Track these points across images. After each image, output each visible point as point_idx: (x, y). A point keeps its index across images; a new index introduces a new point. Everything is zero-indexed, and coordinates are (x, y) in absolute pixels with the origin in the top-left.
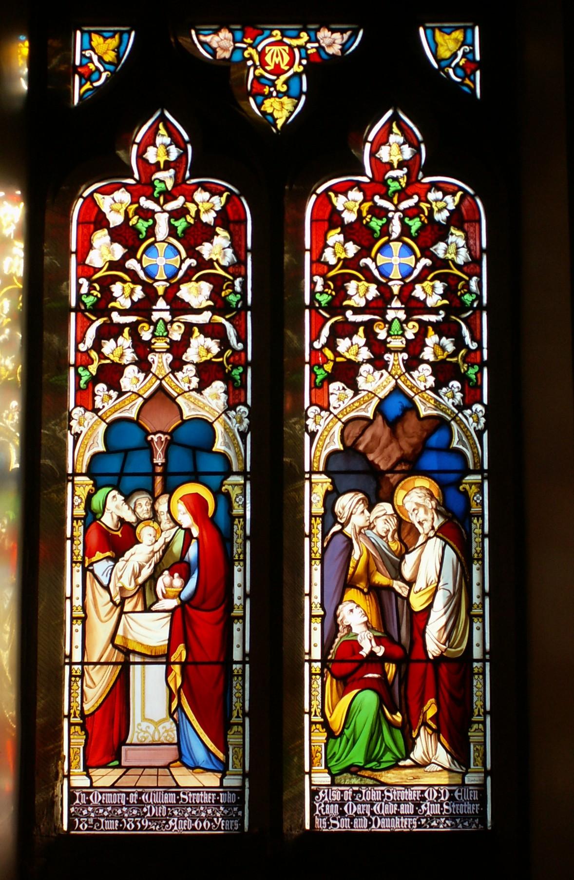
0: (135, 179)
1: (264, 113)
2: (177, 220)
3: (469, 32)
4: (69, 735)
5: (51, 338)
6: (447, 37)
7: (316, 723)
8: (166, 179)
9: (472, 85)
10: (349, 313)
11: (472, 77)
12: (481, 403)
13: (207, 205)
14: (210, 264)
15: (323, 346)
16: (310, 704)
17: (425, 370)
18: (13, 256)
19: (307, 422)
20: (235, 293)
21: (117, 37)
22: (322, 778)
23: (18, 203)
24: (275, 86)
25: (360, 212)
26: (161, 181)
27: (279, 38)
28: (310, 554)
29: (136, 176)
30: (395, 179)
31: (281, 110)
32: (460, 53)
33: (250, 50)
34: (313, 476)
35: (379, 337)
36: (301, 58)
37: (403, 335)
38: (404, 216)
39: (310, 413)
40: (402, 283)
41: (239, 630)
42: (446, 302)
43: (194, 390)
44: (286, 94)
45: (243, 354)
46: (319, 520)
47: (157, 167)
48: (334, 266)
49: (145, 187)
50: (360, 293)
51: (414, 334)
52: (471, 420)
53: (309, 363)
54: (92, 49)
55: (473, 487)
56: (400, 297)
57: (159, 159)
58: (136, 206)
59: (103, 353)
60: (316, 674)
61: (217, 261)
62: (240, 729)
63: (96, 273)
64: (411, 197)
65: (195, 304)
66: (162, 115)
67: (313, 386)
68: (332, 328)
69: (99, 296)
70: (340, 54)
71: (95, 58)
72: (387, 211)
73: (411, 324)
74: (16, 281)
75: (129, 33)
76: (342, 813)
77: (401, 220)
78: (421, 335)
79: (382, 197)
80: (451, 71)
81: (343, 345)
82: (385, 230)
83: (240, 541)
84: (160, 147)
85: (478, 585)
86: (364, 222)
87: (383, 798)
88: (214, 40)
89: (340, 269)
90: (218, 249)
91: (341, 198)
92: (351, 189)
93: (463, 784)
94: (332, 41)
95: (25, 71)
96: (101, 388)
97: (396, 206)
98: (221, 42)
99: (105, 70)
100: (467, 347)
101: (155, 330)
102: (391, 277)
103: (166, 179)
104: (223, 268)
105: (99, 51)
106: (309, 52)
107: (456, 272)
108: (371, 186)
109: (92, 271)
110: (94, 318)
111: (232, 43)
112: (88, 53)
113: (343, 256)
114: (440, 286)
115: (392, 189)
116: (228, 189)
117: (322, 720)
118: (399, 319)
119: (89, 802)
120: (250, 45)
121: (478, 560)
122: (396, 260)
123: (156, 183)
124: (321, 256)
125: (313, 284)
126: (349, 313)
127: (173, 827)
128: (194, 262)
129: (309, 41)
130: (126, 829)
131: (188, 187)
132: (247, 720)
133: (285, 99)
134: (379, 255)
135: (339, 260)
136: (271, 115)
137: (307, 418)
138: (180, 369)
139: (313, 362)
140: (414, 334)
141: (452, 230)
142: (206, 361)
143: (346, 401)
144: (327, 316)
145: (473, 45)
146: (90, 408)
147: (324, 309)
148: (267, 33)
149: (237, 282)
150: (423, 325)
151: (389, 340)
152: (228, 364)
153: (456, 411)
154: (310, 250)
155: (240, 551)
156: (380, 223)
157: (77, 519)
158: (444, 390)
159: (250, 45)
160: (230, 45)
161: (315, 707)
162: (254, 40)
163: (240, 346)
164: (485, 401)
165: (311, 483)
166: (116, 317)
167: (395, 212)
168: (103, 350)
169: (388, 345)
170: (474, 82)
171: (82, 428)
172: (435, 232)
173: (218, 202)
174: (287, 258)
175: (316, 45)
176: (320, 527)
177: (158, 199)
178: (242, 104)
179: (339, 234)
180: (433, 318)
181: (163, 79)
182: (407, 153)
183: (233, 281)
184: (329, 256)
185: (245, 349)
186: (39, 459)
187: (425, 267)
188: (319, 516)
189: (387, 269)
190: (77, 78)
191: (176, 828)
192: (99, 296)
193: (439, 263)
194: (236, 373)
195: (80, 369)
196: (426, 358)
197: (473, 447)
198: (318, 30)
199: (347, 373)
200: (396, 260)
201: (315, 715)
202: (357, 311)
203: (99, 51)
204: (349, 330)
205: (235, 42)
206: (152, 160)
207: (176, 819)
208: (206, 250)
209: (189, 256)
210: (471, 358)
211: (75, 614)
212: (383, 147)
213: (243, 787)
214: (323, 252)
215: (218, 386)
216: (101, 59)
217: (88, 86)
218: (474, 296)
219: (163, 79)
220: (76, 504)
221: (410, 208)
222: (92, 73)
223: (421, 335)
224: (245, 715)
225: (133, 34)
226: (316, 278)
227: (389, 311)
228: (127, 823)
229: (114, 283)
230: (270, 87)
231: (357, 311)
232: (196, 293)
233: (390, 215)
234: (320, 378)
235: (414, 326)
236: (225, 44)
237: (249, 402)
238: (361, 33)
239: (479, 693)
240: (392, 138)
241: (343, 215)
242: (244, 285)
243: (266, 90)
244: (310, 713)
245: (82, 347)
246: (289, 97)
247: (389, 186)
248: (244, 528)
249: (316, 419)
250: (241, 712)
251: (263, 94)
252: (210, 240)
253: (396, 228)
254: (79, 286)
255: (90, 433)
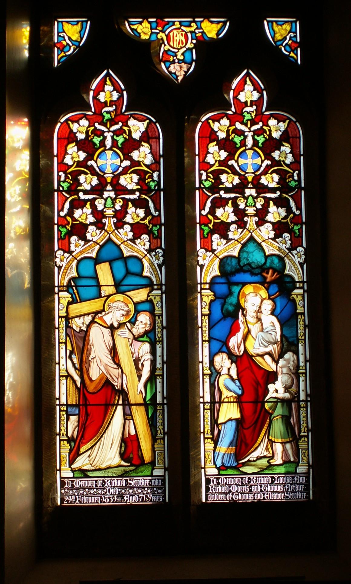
0: (92, 112)
1: (170, 73)
2: (117, 136)
3: (294, 24)
4: (204, 444)
5: (44, 208)
6: (280, 27)
7: (208, 438)
8: (250, 111)
9: (295, 57)
10: (222, 192)
11: (295, 52)
12: (302, 246)
13: (137, 128)
14: (138, 163)
15: (208, 213)
16: (204, 427)
17: (127, 228)
18: (22, 160)
19: (198, 259)
20: (153, 181)
21: (80, 24)
22: (67, 473)
23: (25, 125)
24: (176, 56)
25: (87, 132)
26: (248, 113)
27: (178, 26)
28: (202, 338)
29: (93, 110)
30: (108, 112)
31: (178, 71)
32: (288, 37)
33: (161, 34)
34: (203, 291)
35: (240, 207)
36: (192, 39)
37: (255, 206)
38: (114, 135)
39: (200, 253)
40: (112, 175)
41: (303, 381)
42: (139, 187)
43: (271, 239)
44: (183, 61)
45: (159, 218)
46: (207, 318)
47: (105, 104)
48: (72, 166)
49: (98, 117)
50: (87, 181)
51: (262, 205)
52: (296, 257)
53: (57, 224)
54: (64, 32)
55: (299, 296)
56: (111, 184)
57: (247, 99)
58: (93, 128)
59: (217, 217)
60: (207, 409)
61: (283, 161)
62: (306, 439)
63: (69, 169)
64: (117, 124)
65: (130, 187)
66: (108, 72)
67: (202, 237)
68: (71, 203)
69: (213, 181)
70: (216, 37)
71: (66, 38)
72: (103, 132)
73: (259, 199)
74: (24, 174)
75: (87, 22)
76: (250, 491)
77: (253, 137)
78: (125, 207)
79: (99, 124)
80: (283, 49)
81: (219, 212)
82: (243, 143)
83: (302, 328)
84: (107, 91)
85: (302, 355)
86: (90, 139)
87: (126, 485)
88: (139, 28)
89: (75, 167)
90: (143, 155)
91: (76, 125)
92: (81, 119)
93: (296, 473)
94: (211, 29)
95: (27, 46)
96: (216, 237)
97: (249, 129)
98: (143, 29)
99: (73, 45)
100: (294, 213)
101: (247, 202)
102: (106, 172)
103: (250, 111)
104: (146, 166)
105: (71, 32)
106: (197, 35)
107: (286, 168)
108: (235, 116)
109: (209, 166)
110: (210, 194)
111: (150, 30)
112: (62, 34)
113: (77, 160)
114: (135, 178)
115: (106, 118)
116: (288, 118)
117: (211, 436)
118: (111, 198)
119: (73, 486)
120: (161, 31)
121: (159, 342)
122: (250, 162)
123: (245, 114)
124: (205, 159)
125: (59, 177)
126: (81, 194)
127: (127, 500)
128: (269, 162)
129: (197, 28)
130: (104, 502)
131: (126, 117)
132: (310, 434)
133: (183, 64)
134: (239, 158)
135: (75, 162)
136: (175, 73)
137: (56, 257)
138: (122, 227)
139: (201, 223)
140: (262, 205)
141: (143, 143)
142: (278, 221)
143: (80, 247)
144: (68, 196)
145: (296, 32)
146: (210, 249)
147: (66, 191)
148: (171, 24)
149: (155, 175)
150: (267, 201)
151: (247, 208)
152: (291, 223)
153: (288, 251)
154: (199, 155)
155: (302, 334)
156: (99, 139)
157: (205, 315)
158: (139, 240)
159: (161, 31)
160: (148, 31)
161: (63, 430)
162: (163, 28)
163: (298, 213)
164: (304, 245)
165: (201, 296)
166: (82, 196)
167: (249, 132)
168: (74, 215)
169: (246, 212)
170: (297, 55)
171: (62, 263)
172: (131, 145)
173: (283, 126)
174: (186, 160)
175: (201, 31)
176: (207, 321)
177: (247, 123)
178: (158, 66)
179: (216, 145)
180: (132, 197)
181: (111, 50)
182: (256, 96)
183: (293, 174)
184: (210, 159)
185: (160, 215)
186: (186, 280)
187: (267, 165)
188: (207, 315)
189: (245, 167)
190: (56, 49)
191: (128, 501)
192: (213, 181)
193: (275, 163)
194: (296, 228)
195: (203, 227)
196: (127, 221)
197: (157, 276)
198: (201, 22)
199: (222, 229)
200: (109, 162)
201: (63, 435)
202: (86, 192)
203: (71, 32)
204: (81, 204)
205: (151, 29)
206: (102, 100)
207: (128, 496)
208: (135, 155)
209: (266, 158)
210: (297, 220)
211: (61, 374)
212: (241, 93)
213: (164, 476)
214: (206, 157)
215: (145, 237)
216: (69, 38)
217: (63, 54)
218: (156, 183)
219: (111, 50)
220: (61, 308)
221: (258, 129)
222: (64, 47)
223: (125, 207)
224: (308, 431)
225: (89, 23)
226: (202, 172)
227: (105, 193)
228: (105, 498)
229: (222, 174)
230: (173, 57)
231: (86, 192)
232: (129, 181)
233: (246, 134)
234: (63, 233)
235: (120, 201)
236: (146, 30)
237: (163, 246)
238: (228, 24)
239: (161, 421)
240: (246, 87)
241: (77, 135)
242: (299, 175)
243: (171, 59)
244: (204, 433)
245: (204, 213)
246: (185, 63)
247: (244, 116)
248: (162, 322)
249: (203, 257)
250: (306, 429)
251: (169, 61)
252: (137, 148)
253: (249, 142)
254: (201, 175)
255: (211, 263)
